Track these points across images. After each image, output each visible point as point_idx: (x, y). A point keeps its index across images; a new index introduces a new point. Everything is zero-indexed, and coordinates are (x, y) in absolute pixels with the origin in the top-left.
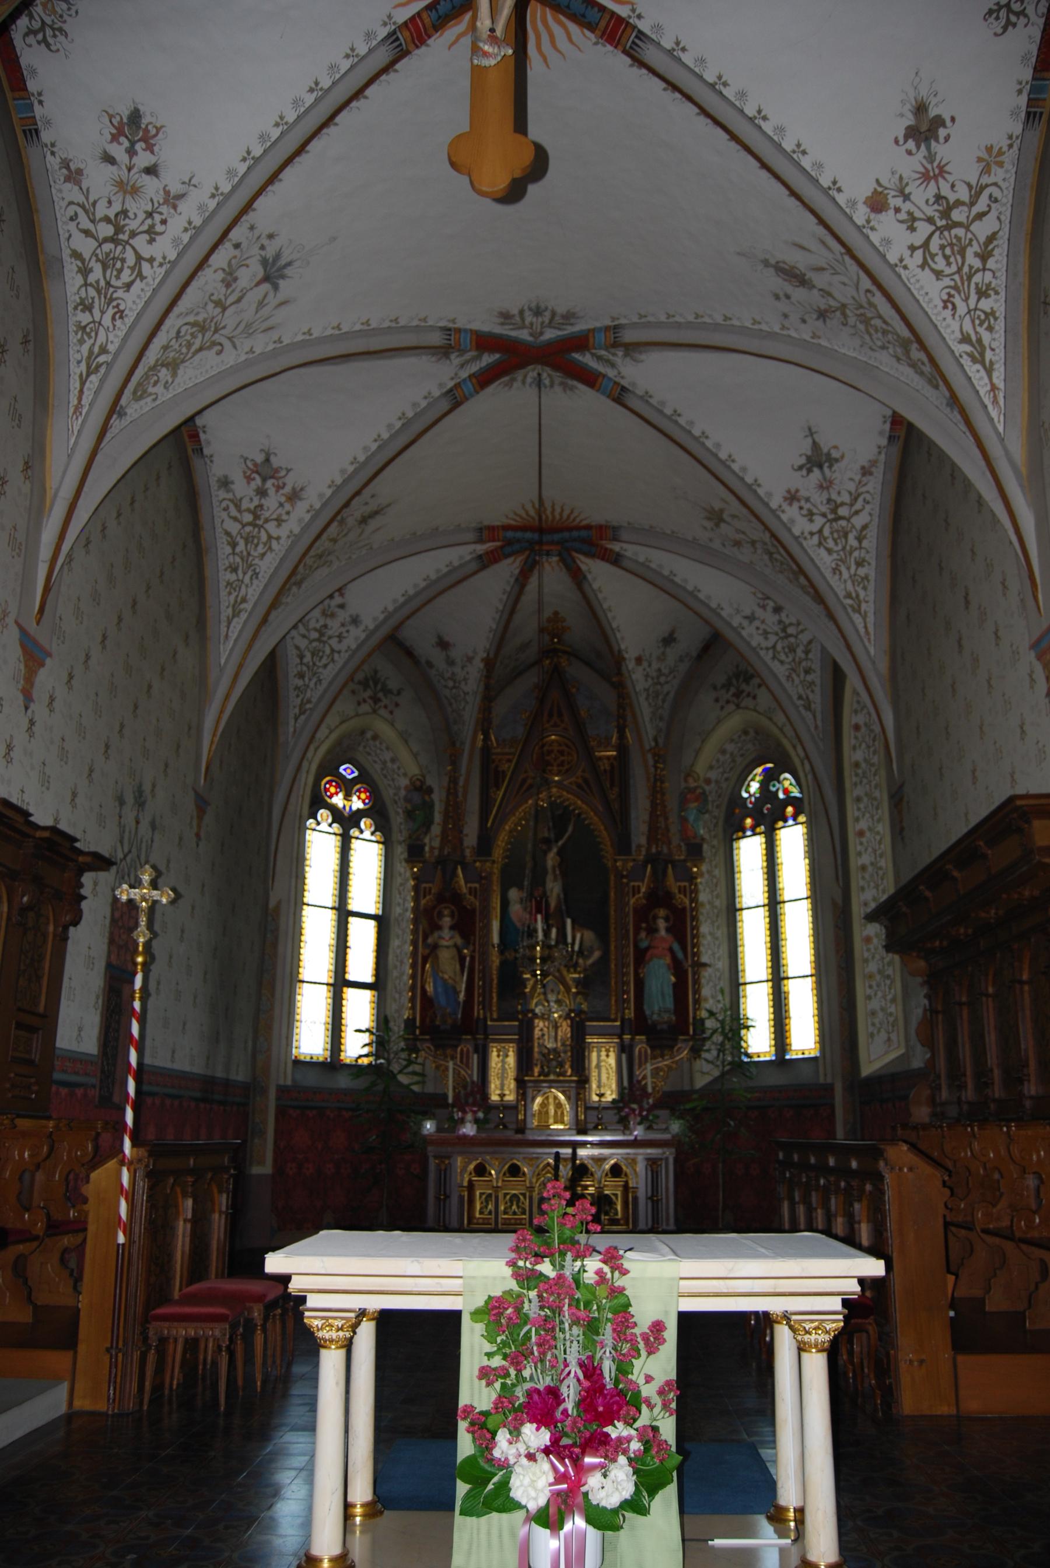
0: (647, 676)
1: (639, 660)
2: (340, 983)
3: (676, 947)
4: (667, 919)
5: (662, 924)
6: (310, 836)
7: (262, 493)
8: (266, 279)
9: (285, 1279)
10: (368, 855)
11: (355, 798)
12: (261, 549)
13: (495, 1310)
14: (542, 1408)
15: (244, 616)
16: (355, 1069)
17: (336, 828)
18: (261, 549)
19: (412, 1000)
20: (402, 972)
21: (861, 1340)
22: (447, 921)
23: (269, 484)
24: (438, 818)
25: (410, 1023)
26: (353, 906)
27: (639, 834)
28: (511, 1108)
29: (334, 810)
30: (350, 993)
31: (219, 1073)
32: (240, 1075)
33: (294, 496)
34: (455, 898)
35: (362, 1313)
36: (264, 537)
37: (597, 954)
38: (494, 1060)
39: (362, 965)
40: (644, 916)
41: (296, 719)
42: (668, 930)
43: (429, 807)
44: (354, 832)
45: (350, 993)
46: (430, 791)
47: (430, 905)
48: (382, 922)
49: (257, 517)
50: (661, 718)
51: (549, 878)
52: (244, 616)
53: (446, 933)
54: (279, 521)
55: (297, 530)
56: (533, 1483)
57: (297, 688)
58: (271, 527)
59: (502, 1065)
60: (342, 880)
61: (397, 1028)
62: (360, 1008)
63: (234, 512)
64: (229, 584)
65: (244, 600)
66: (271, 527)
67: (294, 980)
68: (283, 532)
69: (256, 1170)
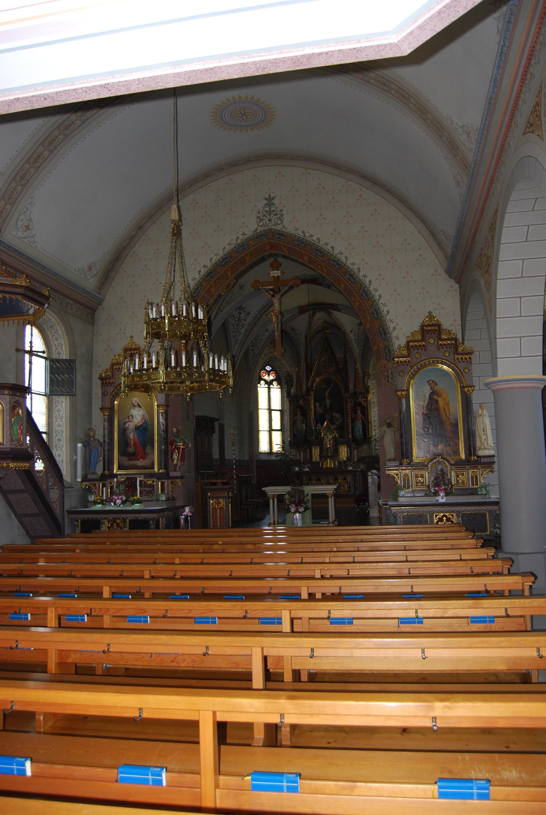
0: (354, 335)
1: (351, 331)
2: (271, 430)
3: (363, 417)
4: (360, 410)
5: (359, 411)
6: (259, 389)
7: (240, 313)
8: (240, 289)
9: (264, 491)
10: (276, 392)
11: (271, 376)
12: (241, 327)
13: (289, 493)
14: (294, 503)
15: (238, 344)
16: (277, 454)
17: (266, 386)
18: (241, 327)
19: (291, 434)
20: (287, 427)
21: (336, 495)
22: (299, 413)
23: (241, 311)
24: (295, 384)
25: (290, 441)
26: (272, 408)
27: (351, 387)
28: (318, 463)
29: (265, 380)
30: (273, 433)
31: (242, 459)
32: (246, 458)
33: (248, 314)
34: (360, 404)
35: (274, 495)
36: (241, 324)
37: (341, 420)
38: (313, 451)
39: (277, 424)
40: (354, 411)
41: (252, 359)
42: (361, 413)
43: (292, 380)
44: (271, 386)
45: (273, 433)
46: (292, 376)
47: (295, 409)
48: (282, 411)
49: (239, 319)
50: (360, 346)
51: (327, 399)
52: (238, 344)
53: (299, 416)
54: (245, 320)
55: (250, 322)
56: (293, 510)
57: (252, 350)
58: (243, 321)
59: (316, 452)
60: (270, 399)
61: (287, 442)
62: (277, 437)
63: (233, 318)
64: (233, 336)
65: (238, 340)
66: (243, 321)
67: (258, 431)
68: (246, 323)
69: (253, 482)
